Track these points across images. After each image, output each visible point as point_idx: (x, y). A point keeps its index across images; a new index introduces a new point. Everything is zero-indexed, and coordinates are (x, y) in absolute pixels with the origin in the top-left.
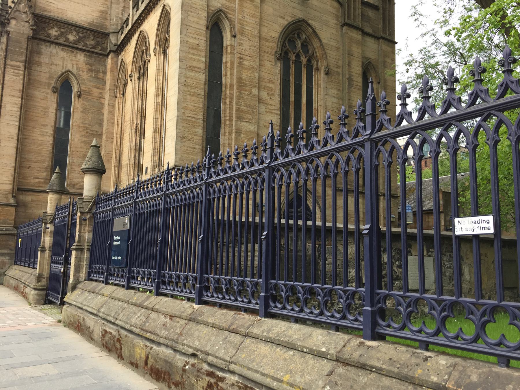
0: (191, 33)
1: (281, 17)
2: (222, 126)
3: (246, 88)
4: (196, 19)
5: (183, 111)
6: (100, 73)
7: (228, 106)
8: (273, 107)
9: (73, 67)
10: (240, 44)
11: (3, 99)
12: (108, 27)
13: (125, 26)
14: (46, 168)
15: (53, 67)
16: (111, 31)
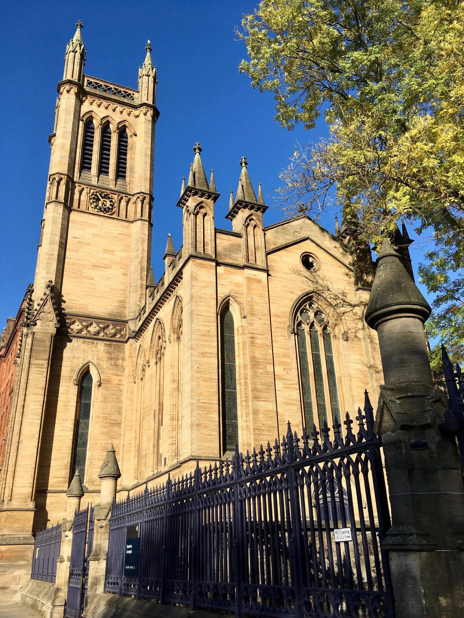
0: (201, 322)
1: (290, 292)
2: (239, 408)
3: (261, 367)
4: (206, 308)
5: (198, 398)
6: (119, 360)
7: (244, 387)
8: (291, 382)
9: (93, 357)
10: (251, 324)
13: (142, 313)
14: (66, 466)
15: (75, 360)
16: (130, 318)
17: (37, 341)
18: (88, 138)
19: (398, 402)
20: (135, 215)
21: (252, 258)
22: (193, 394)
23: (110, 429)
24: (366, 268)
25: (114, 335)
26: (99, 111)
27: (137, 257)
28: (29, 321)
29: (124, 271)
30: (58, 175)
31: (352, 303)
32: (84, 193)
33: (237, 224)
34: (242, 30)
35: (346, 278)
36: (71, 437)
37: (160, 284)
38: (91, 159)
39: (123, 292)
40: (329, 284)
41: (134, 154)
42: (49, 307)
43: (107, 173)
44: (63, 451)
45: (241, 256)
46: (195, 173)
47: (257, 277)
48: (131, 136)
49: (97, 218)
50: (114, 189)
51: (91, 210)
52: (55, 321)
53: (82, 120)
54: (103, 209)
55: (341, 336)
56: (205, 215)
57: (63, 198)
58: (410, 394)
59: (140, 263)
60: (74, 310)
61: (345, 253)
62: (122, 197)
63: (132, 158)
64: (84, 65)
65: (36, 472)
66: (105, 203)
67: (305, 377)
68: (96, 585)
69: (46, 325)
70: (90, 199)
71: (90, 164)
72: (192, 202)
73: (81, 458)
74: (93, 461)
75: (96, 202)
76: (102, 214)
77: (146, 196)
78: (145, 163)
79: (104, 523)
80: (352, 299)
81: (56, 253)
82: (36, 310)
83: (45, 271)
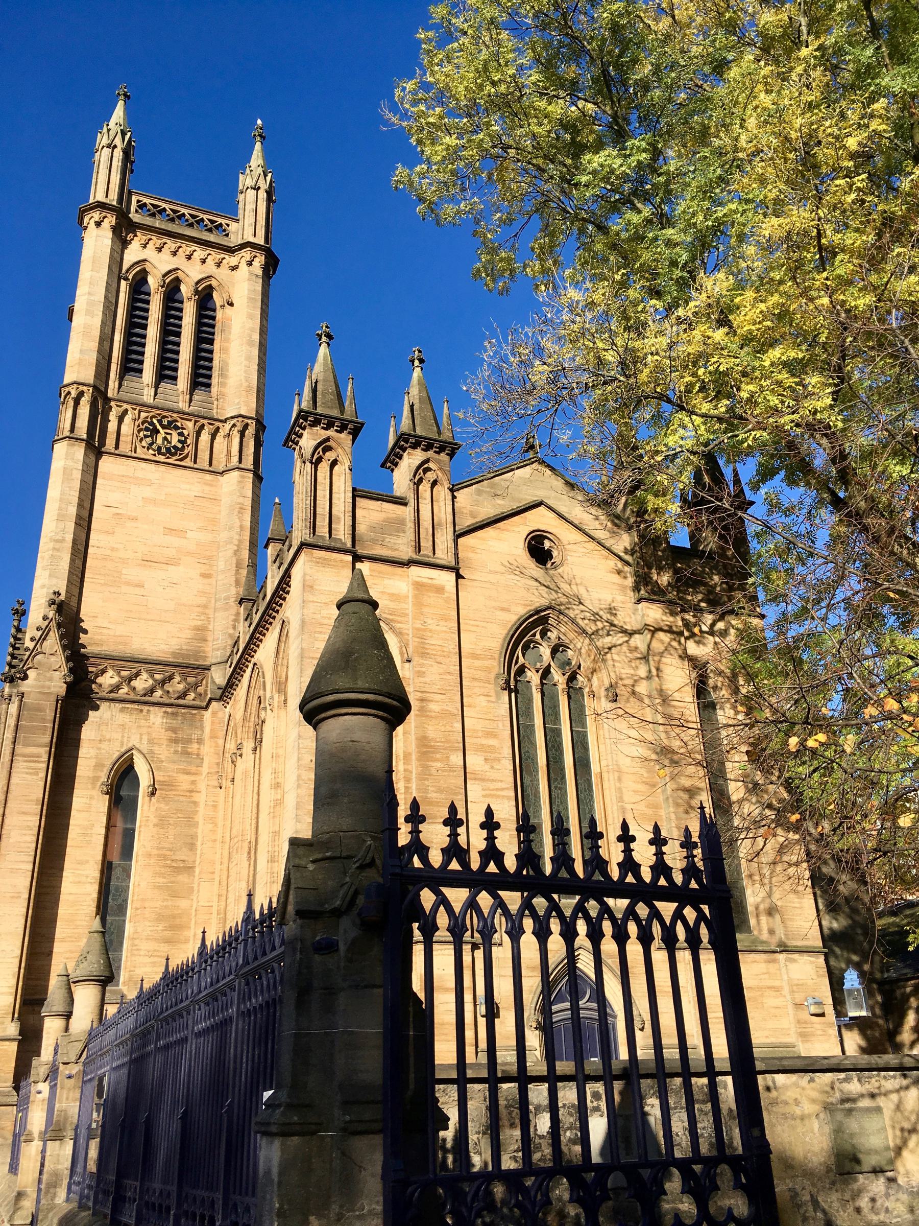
1: (503, 609)
3: (438, 756)
8: (499, 785)
9: (141, 739)
11: (6, 821)
12: (210, 654)
15: (104, 745)
16: (214, 661)
17: (29, 710)
18: (138, 313)
19: (311, 867)
20: (228, 461)
21: (426, 544)
22: (299, 812)
23: (173, 879)
24: (660, 559)
25: (184, 695)
26: (156, 258)
27: (229, 541)
28: (13, 671)
29: (203, 569)
30: (75, 386)
31: (628, 627)
32: (128, 419)
33: (401, 478)
34: (394, 108)
35: (616, 578)
36: (95, 895)
37: (261, 596)
38: (143, 354)
39: (200, 610)
40: (582, 592)
41: (228, 340)
42: (53, 642)
43: (175, 378)
44: (79, 923)
45: (405, 540)
46: (316, 382)
47: (434, 582)
48: (223, 306)
49: (152, 466)
50: (186, 409)
51: (140, 453)
52: (65, 670)
53: (126, 279)
54: (163, 450)
55: (603, 693)
56: (334, 463)
57: (85, 430)
58: (328, 854)
59: (236, 552)
60: (105, 648)
61: (615, 529)
62: (203, 426)
63: (223, 350)
64: (132, 171)
65: (23, 965)
66: (169, 437)
67: (530, 774)
68: (55, 1187)
69: (48, 678)
70: (139, 431)
71: (141, 362)
72: (308, 440)
73: (114, 937)
74: (136, 942)
75: (151, 436)
76: (161, 458)
77: (249, 421)
78: (248, 358)
79: (75, 1069)
80: (627, 620)
81: (69, 537)
82: (27, 649)
83: (47, 573)
